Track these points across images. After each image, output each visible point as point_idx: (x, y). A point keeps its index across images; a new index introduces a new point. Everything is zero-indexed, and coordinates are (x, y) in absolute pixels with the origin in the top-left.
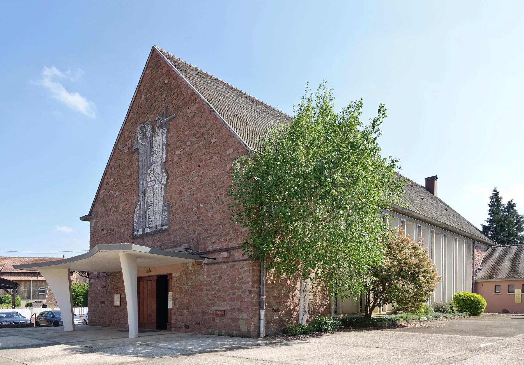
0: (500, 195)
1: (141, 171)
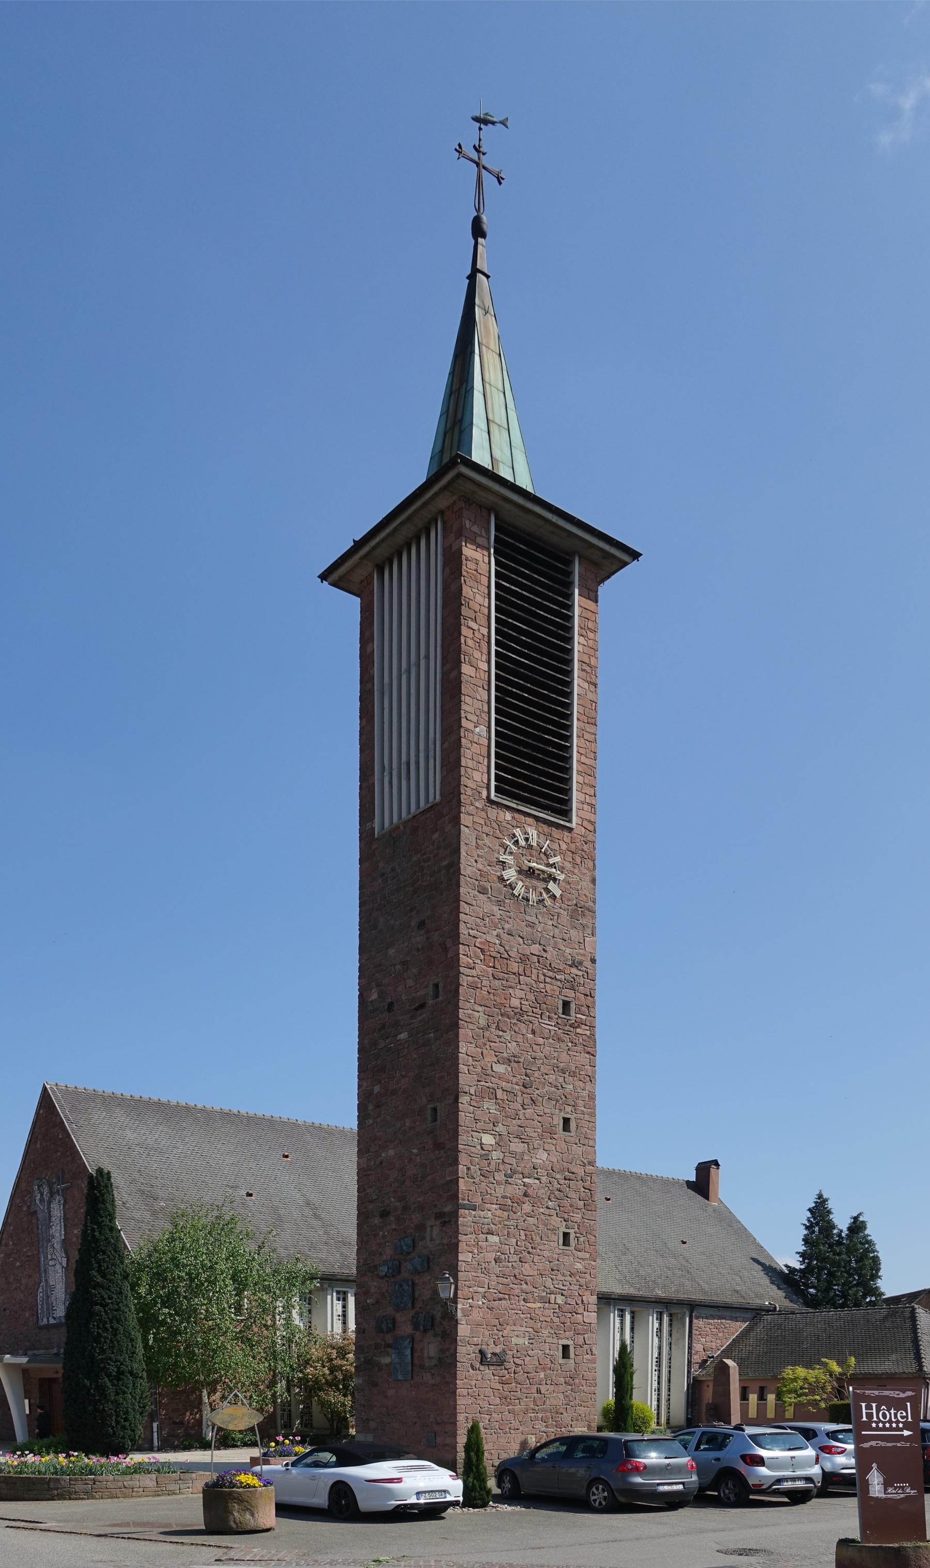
0: (830, 1205)
1: (41, 1245)
